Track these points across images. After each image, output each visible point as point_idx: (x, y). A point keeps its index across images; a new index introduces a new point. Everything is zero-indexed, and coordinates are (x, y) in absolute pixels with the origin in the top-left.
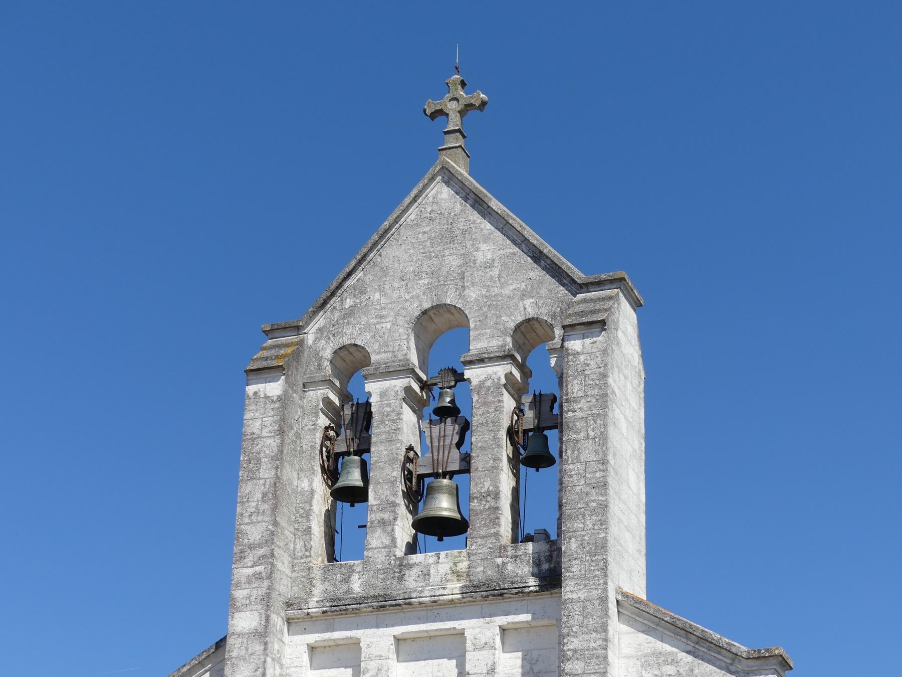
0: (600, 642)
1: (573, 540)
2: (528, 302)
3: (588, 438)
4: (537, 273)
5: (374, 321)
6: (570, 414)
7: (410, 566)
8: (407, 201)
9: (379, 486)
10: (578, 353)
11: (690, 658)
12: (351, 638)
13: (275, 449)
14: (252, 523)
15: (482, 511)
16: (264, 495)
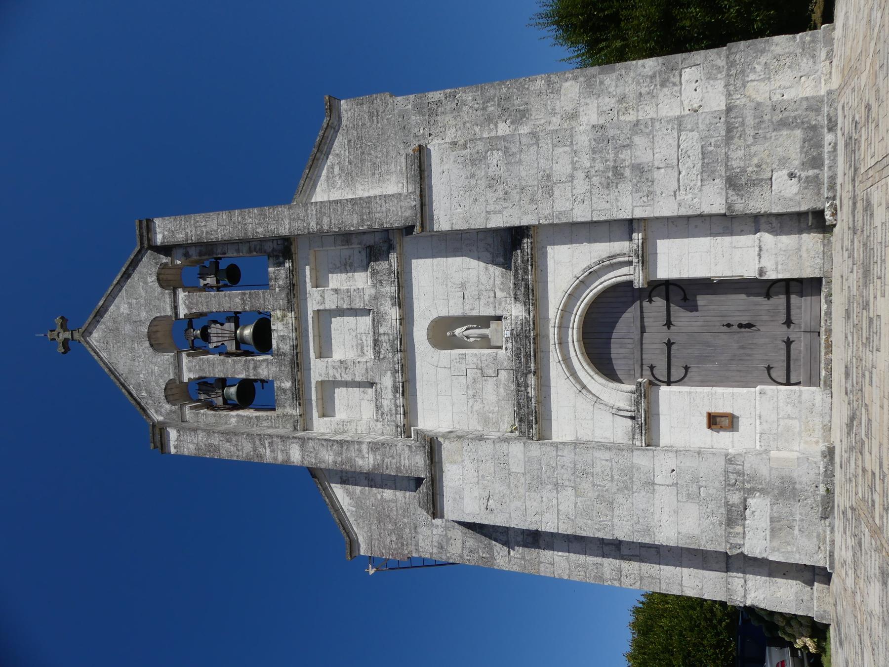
0: (313, 207)
1: (258, 230)
2: (149, 280)
3: (206, 226)
4: (136, 276)
5: (154, 377)
6: (193, 238)
7: (279, 348)
8: (96, 357)
9: (236, 371)
10: (163, 236)
11: (331, 157)
12: (316, 387)
13: (204, 433)
14: (242, 449)
15: (251, 303)
16: (228, 441)
